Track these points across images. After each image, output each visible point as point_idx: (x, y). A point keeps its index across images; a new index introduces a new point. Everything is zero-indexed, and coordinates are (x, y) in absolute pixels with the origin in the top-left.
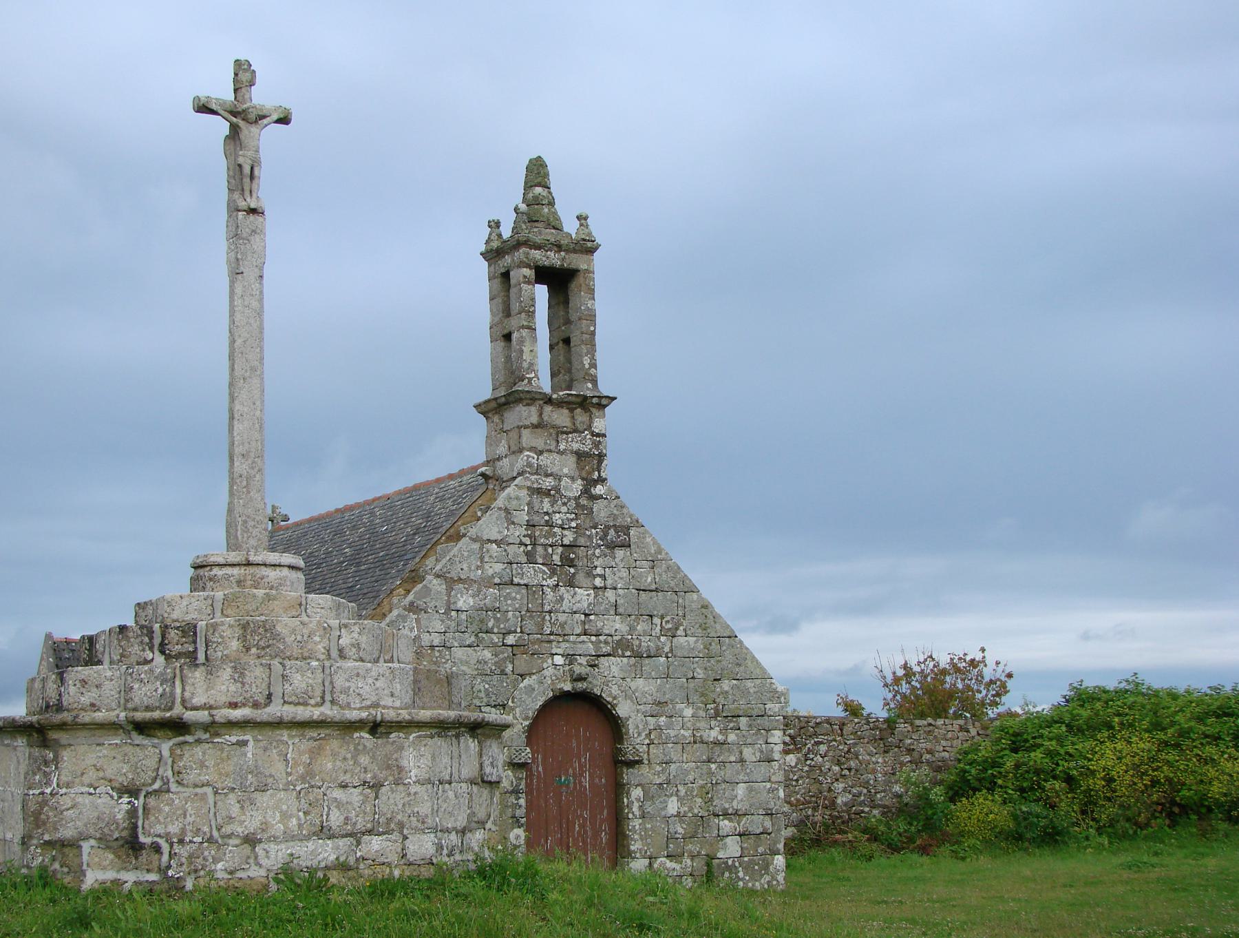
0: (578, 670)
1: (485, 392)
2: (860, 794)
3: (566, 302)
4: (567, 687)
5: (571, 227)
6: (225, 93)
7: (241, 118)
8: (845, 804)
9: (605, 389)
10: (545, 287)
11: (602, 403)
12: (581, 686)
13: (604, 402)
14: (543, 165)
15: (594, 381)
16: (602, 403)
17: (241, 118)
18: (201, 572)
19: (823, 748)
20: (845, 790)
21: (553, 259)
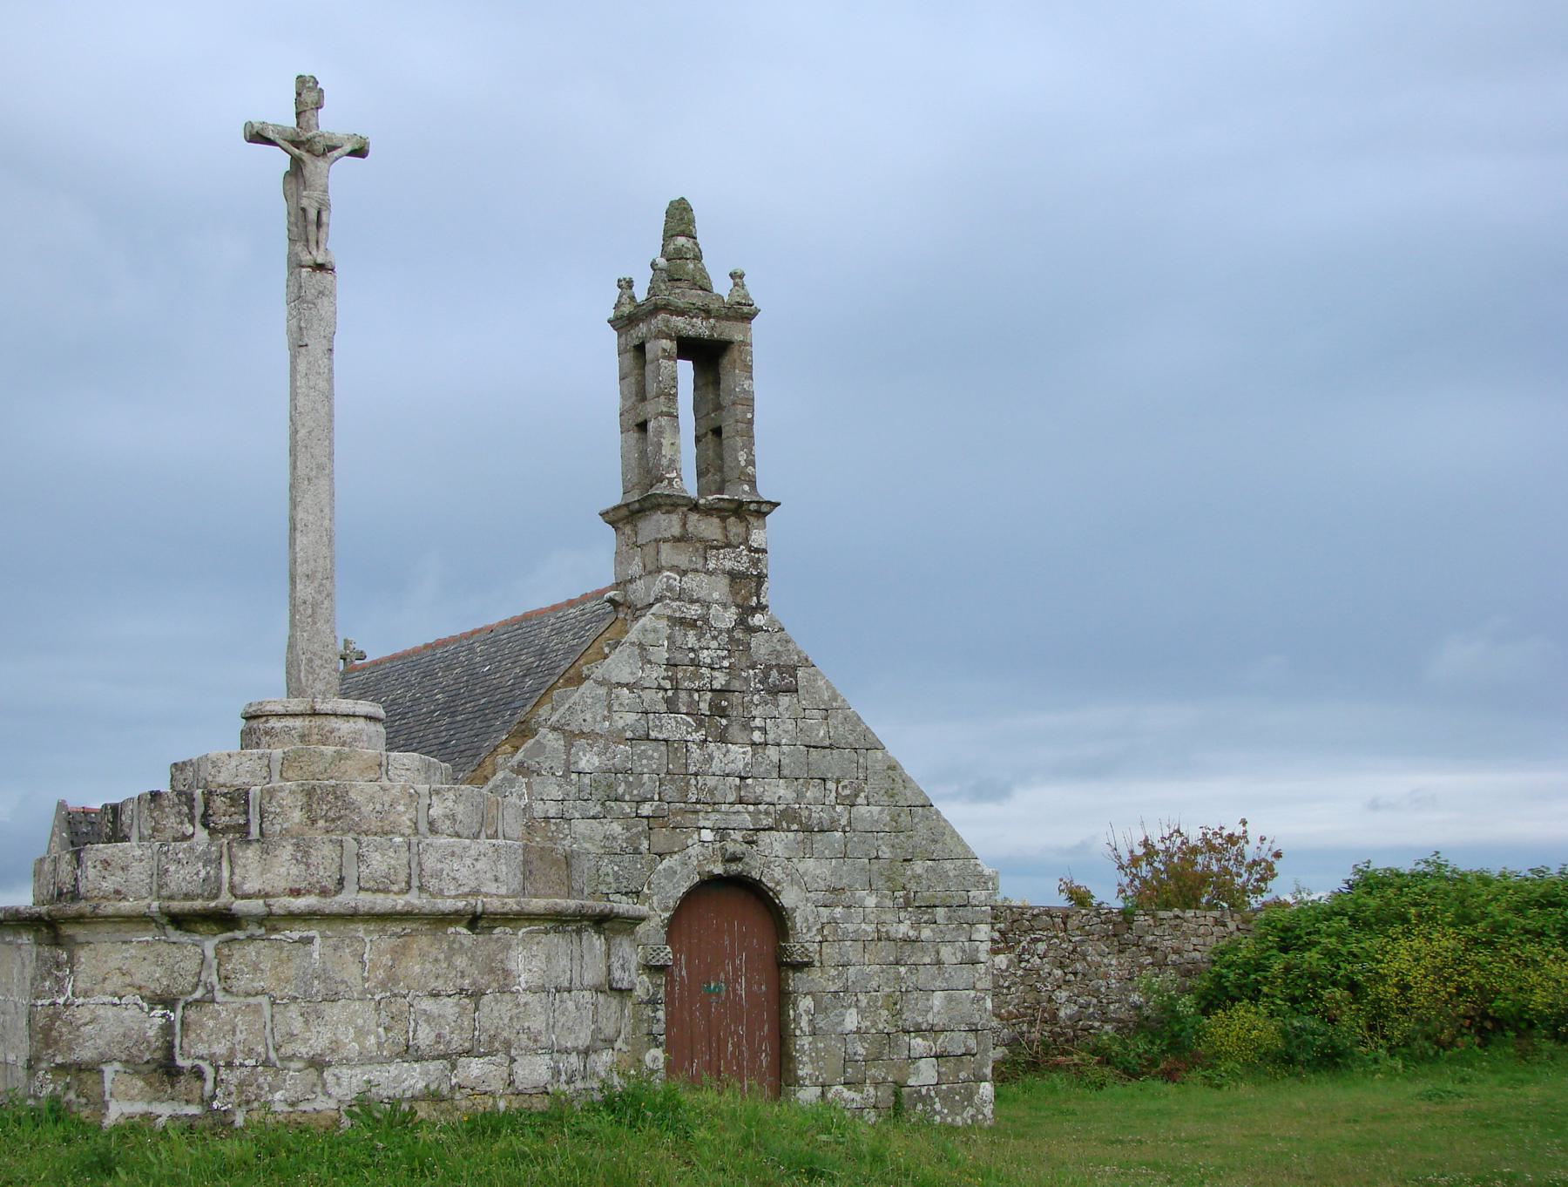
0: (731, 847)
1: (614, 496)
2: (1089, 1005)
3: (717, 382)
4: (718, 869)
5: (722, 287)
6: (285, 117)
7: (304, 149)
8: (1070, 1018)
9: (765, 492)
10: (690, 363)
11: (762, 510)
12: (735, 868)
13: (764, 508)
14: (688, 209)
15: (752, 482)
16: (762, 510)
17: (304, 149)
18: (254, 723)
19: (1041, 947)
20: (1069, 1000)
21: (700, 328)
